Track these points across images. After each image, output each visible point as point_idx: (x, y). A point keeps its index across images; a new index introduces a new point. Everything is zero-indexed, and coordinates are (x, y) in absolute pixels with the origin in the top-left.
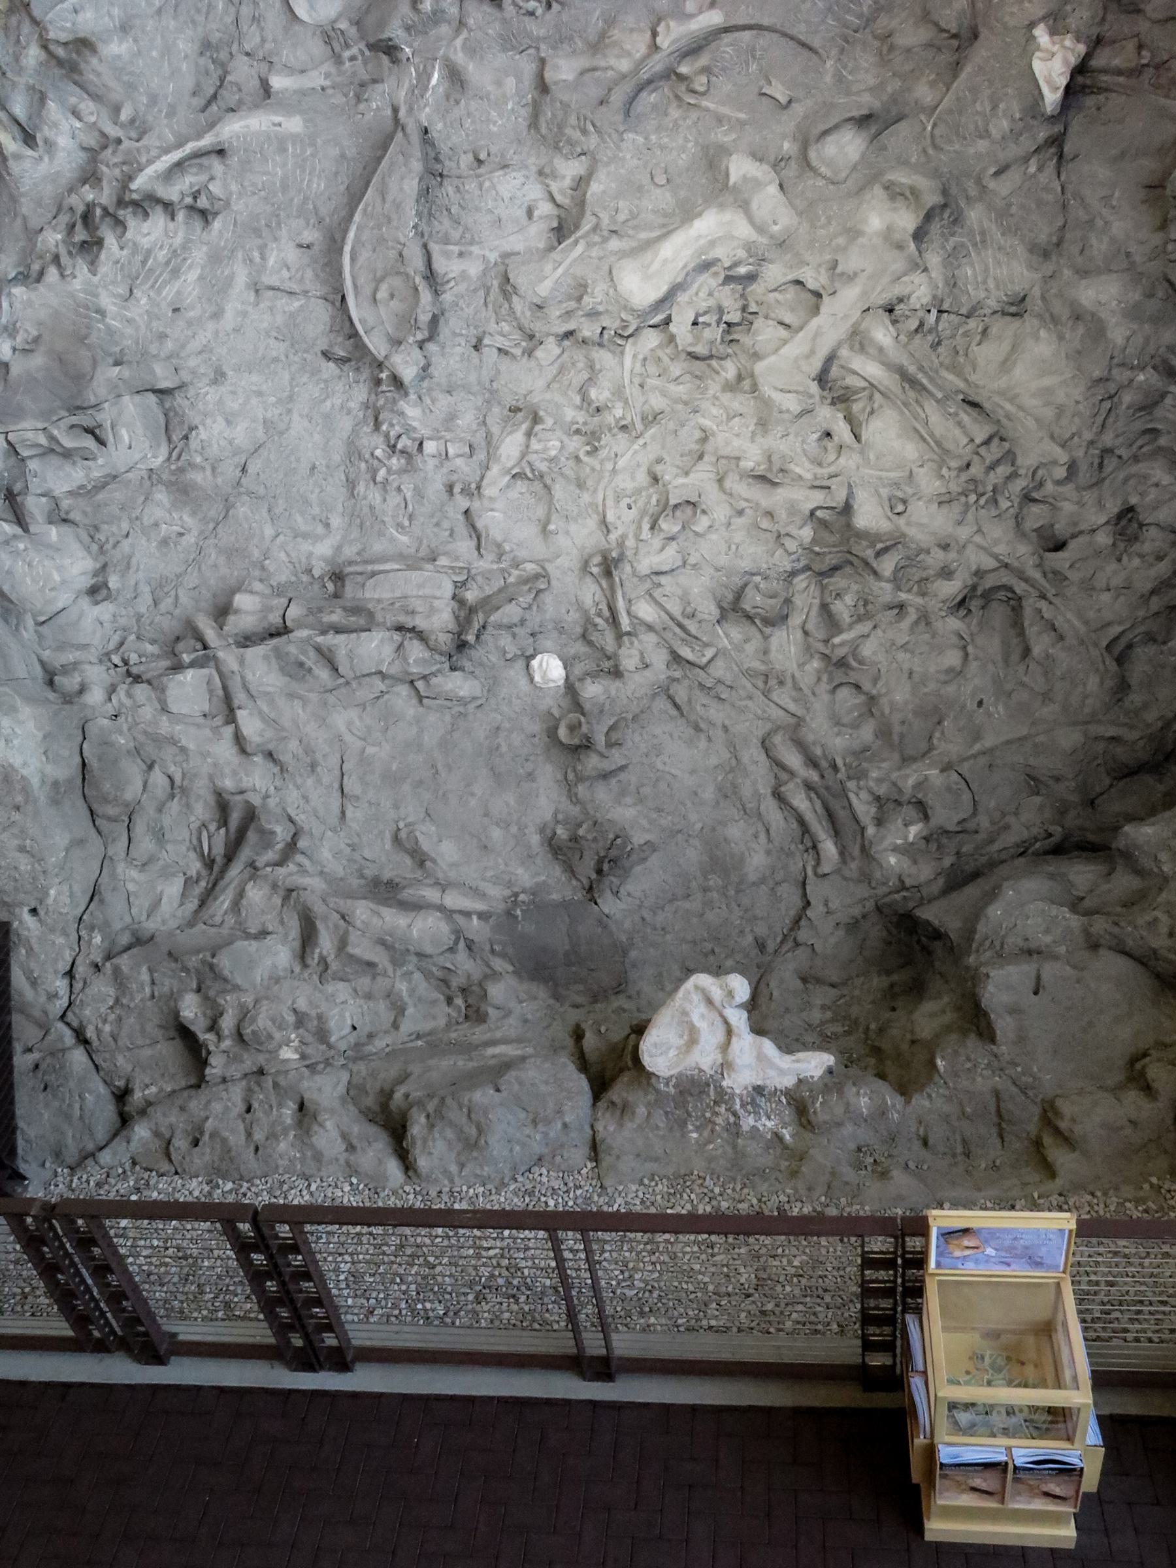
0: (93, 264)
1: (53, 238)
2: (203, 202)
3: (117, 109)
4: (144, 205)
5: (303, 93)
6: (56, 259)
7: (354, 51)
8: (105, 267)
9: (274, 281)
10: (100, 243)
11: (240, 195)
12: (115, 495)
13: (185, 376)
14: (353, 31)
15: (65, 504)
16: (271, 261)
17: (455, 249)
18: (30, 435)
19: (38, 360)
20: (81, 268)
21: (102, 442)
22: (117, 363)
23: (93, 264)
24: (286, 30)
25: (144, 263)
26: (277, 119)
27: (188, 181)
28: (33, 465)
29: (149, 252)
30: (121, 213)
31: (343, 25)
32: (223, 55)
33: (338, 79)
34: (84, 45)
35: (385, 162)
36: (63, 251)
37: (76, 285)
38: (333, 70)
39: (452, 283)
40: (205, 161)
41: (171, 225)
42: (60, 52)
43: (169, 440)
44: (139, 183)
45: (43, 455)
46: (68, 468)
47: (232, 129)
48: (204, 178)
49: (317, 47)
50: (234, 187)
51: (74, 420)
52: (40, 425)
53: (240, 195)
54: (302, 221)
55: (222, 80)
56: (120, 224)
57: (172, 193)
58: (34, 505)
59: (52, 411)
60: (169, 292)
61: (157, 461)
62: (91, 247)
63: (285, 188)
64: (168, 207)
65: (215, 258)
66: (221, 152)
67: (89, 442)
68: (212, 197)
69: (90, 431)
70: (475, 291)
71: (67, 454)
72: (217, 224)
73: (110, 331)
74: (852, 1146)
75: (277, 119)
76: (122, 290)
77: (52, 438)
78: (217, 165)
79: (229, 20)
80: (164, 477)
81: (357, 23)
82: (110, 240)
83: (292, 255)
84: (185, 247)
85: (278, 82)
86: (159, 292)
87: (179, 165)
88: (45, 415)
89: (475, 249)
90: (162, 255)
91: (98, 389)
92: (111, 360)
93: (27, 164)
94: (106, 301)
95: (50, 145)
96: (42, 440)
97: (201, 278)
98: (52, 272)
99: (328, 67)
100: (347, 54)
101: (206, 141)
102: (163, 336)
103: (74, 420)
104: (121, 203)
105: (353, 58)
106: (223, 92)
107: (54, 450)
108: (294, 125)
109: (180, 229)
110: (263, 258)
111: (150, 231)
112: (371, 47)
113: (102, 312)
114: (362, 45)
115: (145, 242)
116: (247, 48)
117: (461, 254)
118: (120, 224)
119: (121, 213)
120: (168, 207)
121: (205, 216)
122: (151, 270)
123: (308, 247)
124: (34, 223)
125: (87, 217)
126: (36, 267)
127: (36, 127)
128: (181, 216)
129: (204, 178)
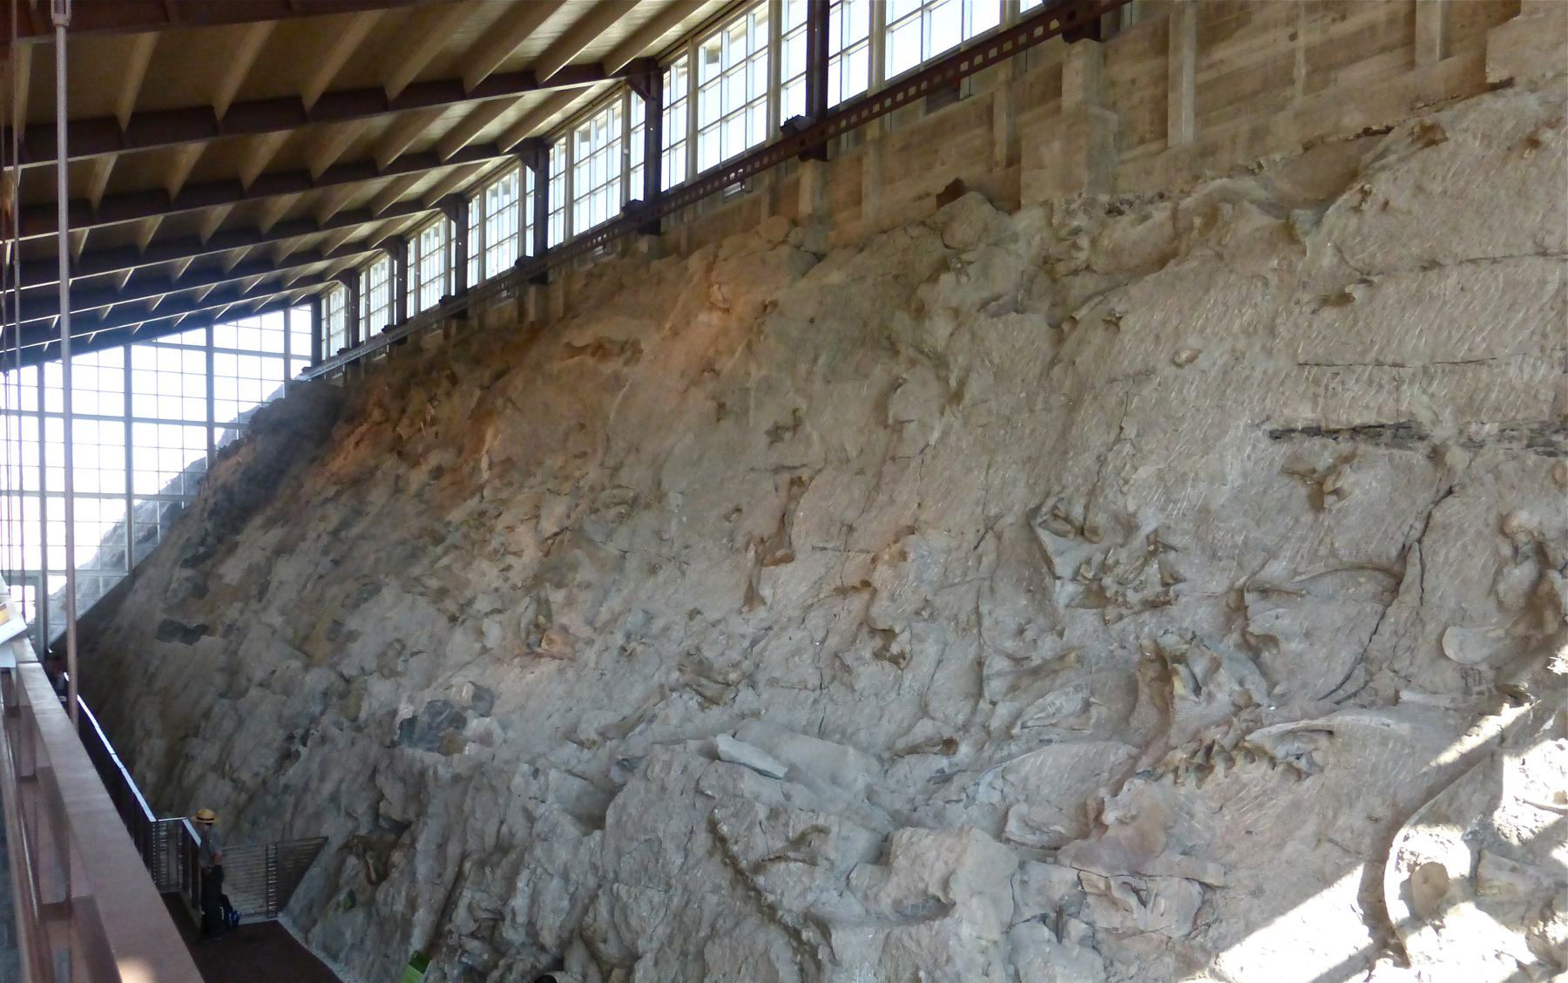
0: (1200, 782)
1: (1180, 756)
2: (1302, 764)
3: (1274, 685)
4: (1253, 754)
5: (1427, 708)
6: (1176, 770)
7: (1483, 687)
8: (1210, 783)
9: (1337, 837)
10: (1211, 768)
11: (1334, 767)
12: (1138, 946)
13: (1231, 880)
14: (1490, 674)
15: (1100, 936)
16: (1340, 822)
17: (1511, 863)
18: (1094, 877)
19: (1128, 832)
20: (1191, 781)
21: (1143, 903)
22: (1183, 853)
23: (1200, 782)
24: (1433, 661)
25: (1238, 792)
26: (1388, 721)
27: (1295, 746)
28: (1090, 900)
29: (1245, 786)
30: (1234, 753)
31: (1483, 667)
32: (1374, 668)
33: (1462, 705)
34: (1270, 640)
35: (1467, 775)
36: (1183, 767)
37: (1183, 791)
38: (1460, 698)
39: (1495, 891)
40: (1315, 736)
41: (1270, 772)
42: (1253, 641)
43: (1195, 922)
44: (1255, 737)
45: (1100, 896)
46: (1112, 912)
47: (1344, 720)
48: (1312, 747)
49: (1451, 678)
50: (1331, 760)
51: (1130, 880)
52: (1104, 874)
53: (1334, 767)
54: (1379, 800)
55: (1366, 683)
56: (1230, 761)
57: (1280, 752)
58: (1076, 928)
59: (1118, 868)
60: (1249, 818)
61: (1178, 933)
62: (1204, 769)
63: (1374, 771)
64: (1273, 762)
65: (1296, 806)
66: (1330, 733)
67: (1133, 901)
68: (1311, 763)
69: (1136, 891)
70: (1516, 904)
71: (1114, 903)
72: (1308, 782)
73: (1191, 830)
74: (391, 636)
75: (1388, 721)
76: (1215, 805)
77: (1108, 887)
78: (1323, 741)
79: (1389, 645)
80: (1178, 948)
81: (1498, 669)
82: (1220, 769)
83: (1359, 822)
84: (1273, 790)
85: (1405, 695)
86: (1242, 815)
87: (1293, 733)
88: (1112, 868)
89: (1531, 870)
90: (1255, 791)
91: (1156, 866)
92: (1180, 849)
93: (1187, 704)
94: (1200, 809)
95: (1210, 696)
96: (1102, 885)
97: (1279, 816)
98: (1171, 776)
99: (1458, 695)
100: (1478, 689)
101: (1320, 722)
102: (1230, 847)
103: (1130, 880)
104: (1236, 746)
105: (1481, 693)
106: (1363, 693)
107: (1105, 895)
108: (1404, 728)
109: (1274, 776)
110: (1335, 817)
111: (1252, 773)
112: (1497, 687)
113: (1192, 816)
114: (1491, 685)
115: (1245, 777)
116: (1396, 667)
117: (1513, 870)
118: (1230, 761)
119: (1234, 753)
120: (1273, 762)
121: (1300, 775)
122: (1242, 799)
123: (1376, 820)
124: (1173, 742)
125: (1209, 749)
126: (1160, 771)
127: (1206, 684)
128: (1280, 769)
129: (1312, 747)
